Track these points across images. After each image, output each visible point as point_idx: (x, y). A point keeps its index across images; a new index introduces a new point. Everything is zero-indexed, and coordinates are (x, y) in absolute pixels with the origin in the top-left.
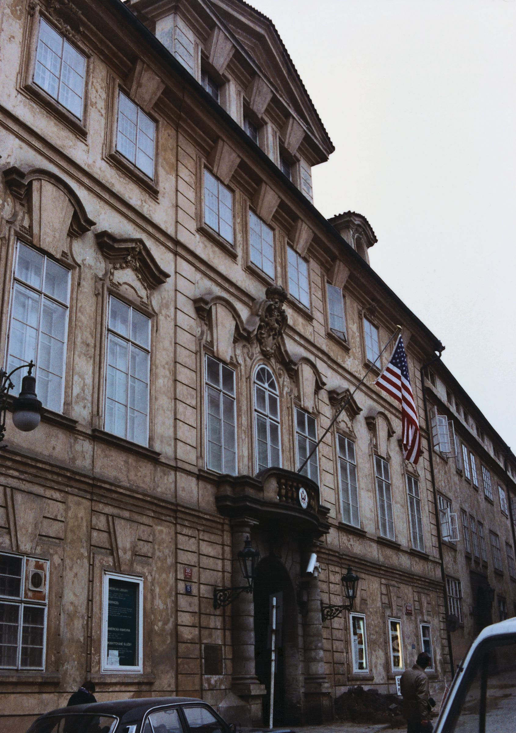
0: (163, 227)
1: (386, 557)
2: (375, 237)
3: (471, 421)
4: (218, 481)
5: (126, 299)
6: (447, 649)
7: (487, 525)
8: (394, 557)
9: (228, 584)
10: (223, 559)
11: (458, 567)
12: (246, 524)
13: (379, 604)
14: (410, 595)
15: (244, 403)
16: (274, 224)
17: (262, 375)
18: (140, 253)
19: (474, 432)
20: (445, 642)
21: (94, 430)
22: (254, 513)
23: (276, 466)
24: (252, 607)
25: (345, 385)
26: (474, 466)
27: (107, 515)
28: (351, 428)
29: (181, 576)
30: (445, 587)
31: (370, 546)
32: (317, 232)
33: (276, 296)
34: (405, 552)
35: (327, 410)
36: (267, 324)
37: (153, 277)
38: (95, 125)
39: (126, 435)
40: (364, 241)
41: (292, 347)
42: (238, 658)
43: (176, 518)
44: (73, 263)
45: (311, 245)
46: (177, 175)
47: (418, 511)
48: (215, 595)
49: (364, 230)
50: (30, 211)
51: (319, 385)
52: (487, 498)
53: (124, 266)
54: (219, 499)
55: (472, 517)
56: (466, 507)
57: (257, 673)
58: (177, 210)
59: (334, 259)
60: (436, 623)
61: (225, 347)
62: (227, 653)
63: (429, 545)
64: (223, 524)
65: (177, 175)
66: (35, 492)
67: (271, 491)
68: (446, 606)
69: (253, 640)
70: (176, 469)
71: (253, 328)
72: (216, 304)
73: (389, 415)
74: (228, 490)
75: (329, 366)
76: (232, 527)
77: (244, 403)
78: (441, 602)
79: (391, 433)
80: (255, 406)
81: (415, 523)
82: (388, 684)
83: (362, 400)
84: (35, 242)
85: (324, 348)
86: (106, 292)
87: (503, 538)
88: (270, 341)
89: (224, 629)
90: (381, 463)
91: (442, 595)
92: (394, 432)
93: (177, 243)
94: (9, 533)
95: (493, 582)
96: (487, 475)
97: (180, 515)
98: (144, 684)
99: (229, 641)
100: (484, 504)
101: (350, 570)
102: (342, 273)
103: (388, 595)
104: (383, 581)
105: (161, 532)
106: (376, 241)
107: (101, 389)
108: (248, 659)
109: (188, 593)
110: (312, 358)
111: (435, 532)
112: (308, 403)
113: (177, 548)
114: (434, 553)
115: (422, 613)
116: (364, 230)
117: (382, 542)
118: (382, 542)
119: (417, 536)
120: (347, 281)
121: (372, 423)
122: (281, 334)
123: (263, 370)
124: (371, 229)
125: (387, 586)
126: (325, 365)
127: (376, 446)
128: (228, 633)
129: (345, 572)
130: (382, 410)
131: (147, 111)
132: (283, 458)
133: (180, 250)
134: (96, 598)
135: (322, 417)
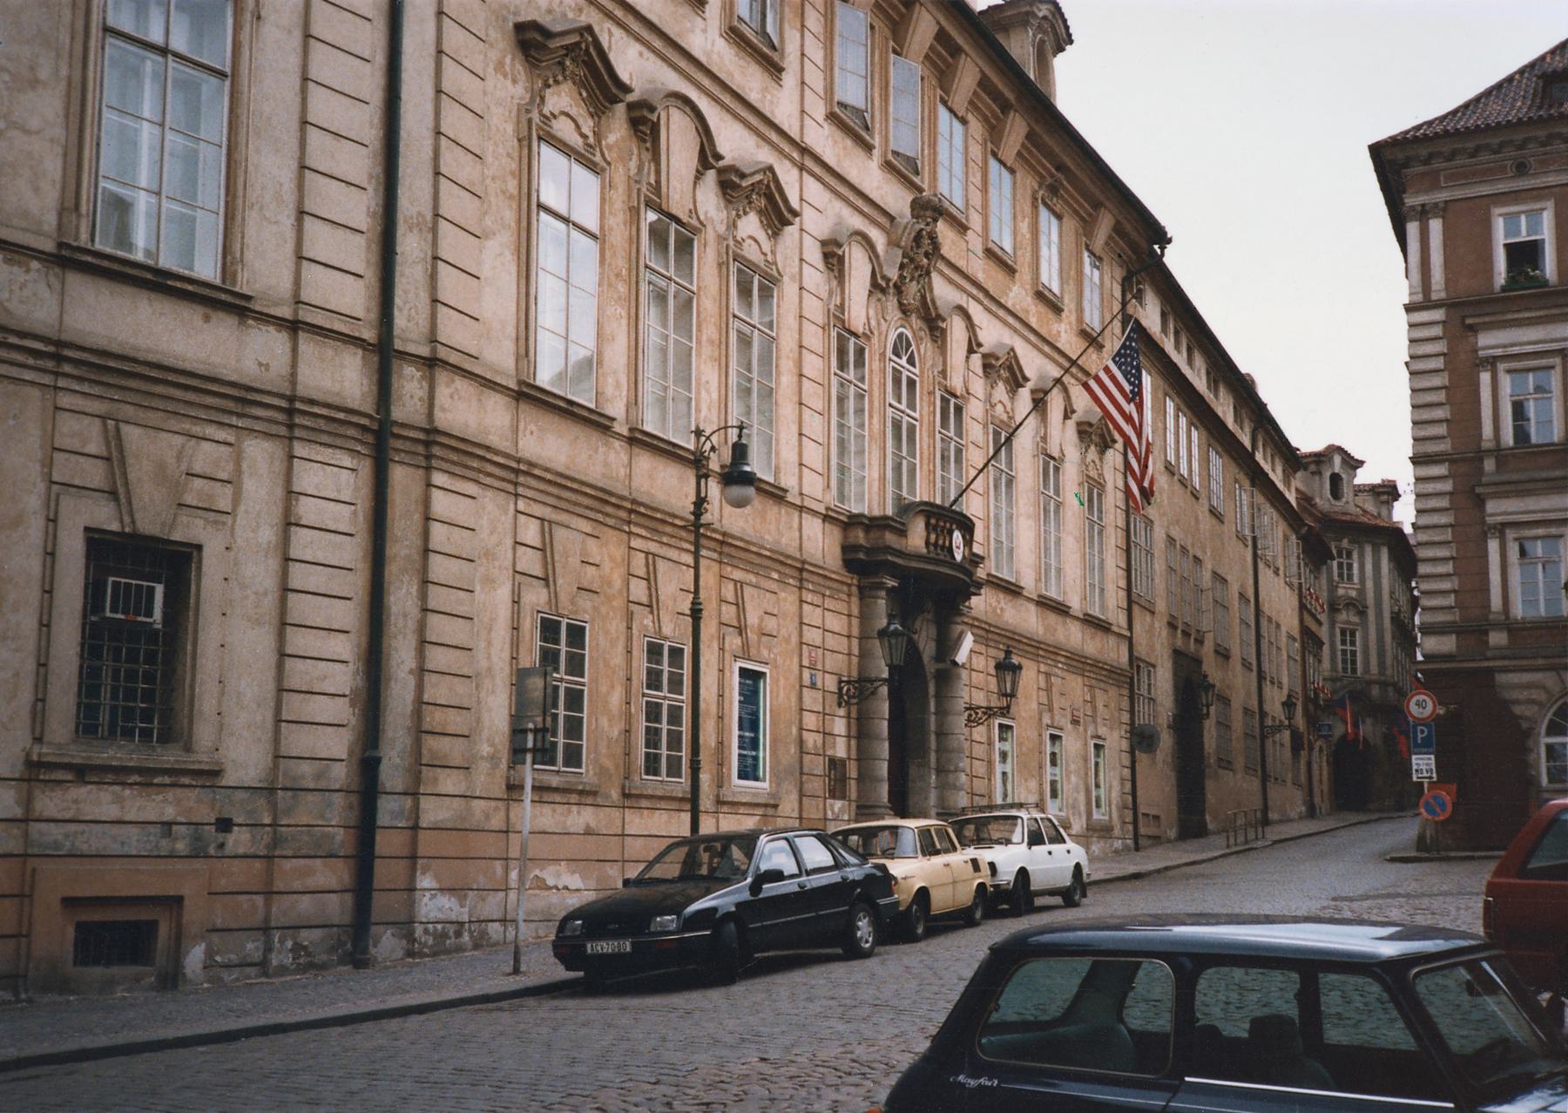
0: (785, 128)
1: (1046, 628)
2: (1070, 36)
3: (1199, 361)
4: (851, 523)
5: (565, 144)
6: (1128, 786)
7: (1208, 565)
8: (1060, 629)
9: (855, 674)
10: (849, 637)
11: (1155, 642)
12: (881, 586)
13: (1034, 706)
14: (1079, 692)
15: (876, 393)
16: (1017, 166)
17: (901, 346)
18: (768, 186)
19: (1200, 382)
20: (1127, 772)
21: (521, 383)
22: (894, 570)
24: (886, 706)
25: (765, 156)
26: (1195, 451)
27: (736, 582)
28: (590, 135)
29: (806, 663)
30: (1132, 679)
31: (1028, 610)
32: (944, 23)
33: (928, 213)
34: (1077, 618)
35: (978, 386)
36: (912, 260)
37: (778, 215)
40: (1048, 47)
41: (944, 292)
42: (865, 778)
45: (975, 93)
46: (803, 26)
47: (1101, 543)
48: (840, 689)
49: (1053, 26)
50: (656, 158)
52: (1213, 512)
53: (560, 78)
54: (847, 549)
55: (1184, 549)
56: (1175, 533)
57: (890, 801)
58: (802, 91)
59: (1005, 107)
60: (1116, 741)
61: (859, 310)
62: (853, 772)
63: (1112, 608)
64: (849, 585)
65: (803, 26)
67: (917, 537)
68: (1132, 712)
69: (886, 754)
70: (801, 509)
71: (893, 274)
73: (703, 104)
74: (860, 536)
75: (987, 309)
76: (860, 588)
77: (876, 393)
78: (1125, 704)
79: (1068, 413)
80: (890, 399)
81: (1047, 548)
82: (29, 780)
83: (1034, 364)
84: (664, 207)
85: (981, 277)
86: (642, 206)
87: (1234, 588)
88: (912, 289)
89: (848, 737)
90: (1050, 463)
91: (1126, 692)
92: (1073, 412)
93: (805, 151)
94: (548, 586)
95: (1210, 667)
96: (1217, 462)
97: (805, 575)
98: (770, 806)
99: (854, 755)
100: (1206, 521)
101: (1008, 653)
102: (1016, 130)
103: (1049, 690)
104: (1043, 668)
105: (785, 600)
106: (1071, 42)
107: (90, 96)
108: (880, 780)
109: (813, 686)
110: (693, 95)
111: (1123, 583)
112: (956, 382)
113: (801, 623)
114: (1119, 619)
115: (1095, 721)
116: (1053, 26)
117: (1047, 604)
118: (1047, 604)
119: (1096, 587)
120: (1023, 145)
121: (834, 255)
122: (928, 273)
123: (900, 336)
124: (1065, 21)
125: (1048, 675)
126: (980, 308)
127: (1044, 439)
128: (853, 742)
129: (1002, 655)
130: (962, 299)
133: (809, 163)
134: (727, 694)
135: (972, 399)
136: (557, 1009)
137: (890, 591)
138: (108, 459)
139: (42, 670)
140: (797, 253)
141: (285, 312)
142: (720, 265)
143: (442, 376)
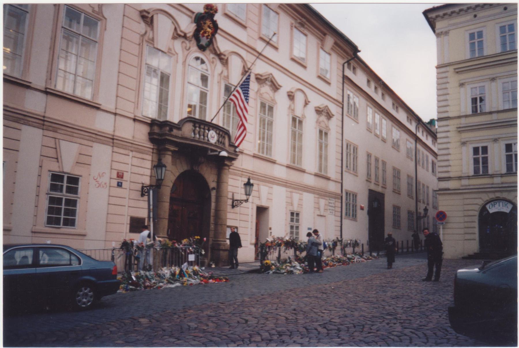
12: (168, 150)
23: (203, 119)
37: (275, 87)
38: (311, 64)
39: (74, 91)
43: (113, 143)
44: (174, 53)
50: (152, 29)
51: (306, 103)
66: (67, 136)
72: (157, 14)
90: (297, 122)
101: (249, 179)
102: (330, 41)
131: (275, 10)
132: (233, 123)
136: (406, 262)
137: (173, 152)
138: (56, 148)
139: (295, 224)
140: (281, 98)
141: (114, 111)
142: (218, 82)
143: (117, 117)
